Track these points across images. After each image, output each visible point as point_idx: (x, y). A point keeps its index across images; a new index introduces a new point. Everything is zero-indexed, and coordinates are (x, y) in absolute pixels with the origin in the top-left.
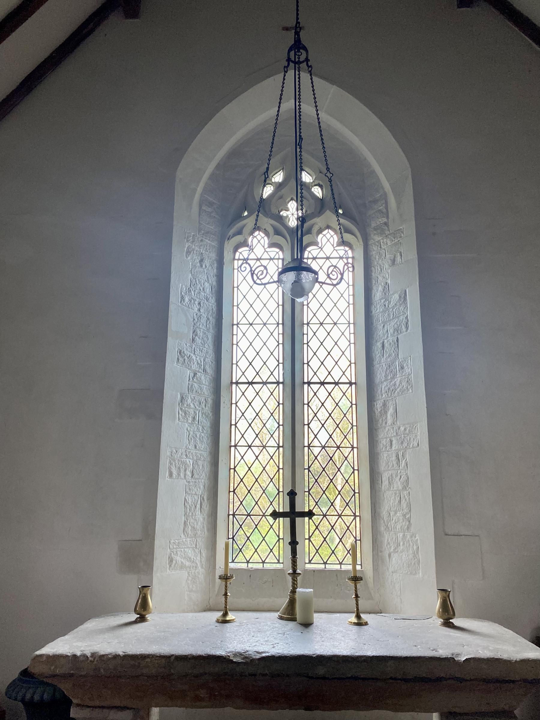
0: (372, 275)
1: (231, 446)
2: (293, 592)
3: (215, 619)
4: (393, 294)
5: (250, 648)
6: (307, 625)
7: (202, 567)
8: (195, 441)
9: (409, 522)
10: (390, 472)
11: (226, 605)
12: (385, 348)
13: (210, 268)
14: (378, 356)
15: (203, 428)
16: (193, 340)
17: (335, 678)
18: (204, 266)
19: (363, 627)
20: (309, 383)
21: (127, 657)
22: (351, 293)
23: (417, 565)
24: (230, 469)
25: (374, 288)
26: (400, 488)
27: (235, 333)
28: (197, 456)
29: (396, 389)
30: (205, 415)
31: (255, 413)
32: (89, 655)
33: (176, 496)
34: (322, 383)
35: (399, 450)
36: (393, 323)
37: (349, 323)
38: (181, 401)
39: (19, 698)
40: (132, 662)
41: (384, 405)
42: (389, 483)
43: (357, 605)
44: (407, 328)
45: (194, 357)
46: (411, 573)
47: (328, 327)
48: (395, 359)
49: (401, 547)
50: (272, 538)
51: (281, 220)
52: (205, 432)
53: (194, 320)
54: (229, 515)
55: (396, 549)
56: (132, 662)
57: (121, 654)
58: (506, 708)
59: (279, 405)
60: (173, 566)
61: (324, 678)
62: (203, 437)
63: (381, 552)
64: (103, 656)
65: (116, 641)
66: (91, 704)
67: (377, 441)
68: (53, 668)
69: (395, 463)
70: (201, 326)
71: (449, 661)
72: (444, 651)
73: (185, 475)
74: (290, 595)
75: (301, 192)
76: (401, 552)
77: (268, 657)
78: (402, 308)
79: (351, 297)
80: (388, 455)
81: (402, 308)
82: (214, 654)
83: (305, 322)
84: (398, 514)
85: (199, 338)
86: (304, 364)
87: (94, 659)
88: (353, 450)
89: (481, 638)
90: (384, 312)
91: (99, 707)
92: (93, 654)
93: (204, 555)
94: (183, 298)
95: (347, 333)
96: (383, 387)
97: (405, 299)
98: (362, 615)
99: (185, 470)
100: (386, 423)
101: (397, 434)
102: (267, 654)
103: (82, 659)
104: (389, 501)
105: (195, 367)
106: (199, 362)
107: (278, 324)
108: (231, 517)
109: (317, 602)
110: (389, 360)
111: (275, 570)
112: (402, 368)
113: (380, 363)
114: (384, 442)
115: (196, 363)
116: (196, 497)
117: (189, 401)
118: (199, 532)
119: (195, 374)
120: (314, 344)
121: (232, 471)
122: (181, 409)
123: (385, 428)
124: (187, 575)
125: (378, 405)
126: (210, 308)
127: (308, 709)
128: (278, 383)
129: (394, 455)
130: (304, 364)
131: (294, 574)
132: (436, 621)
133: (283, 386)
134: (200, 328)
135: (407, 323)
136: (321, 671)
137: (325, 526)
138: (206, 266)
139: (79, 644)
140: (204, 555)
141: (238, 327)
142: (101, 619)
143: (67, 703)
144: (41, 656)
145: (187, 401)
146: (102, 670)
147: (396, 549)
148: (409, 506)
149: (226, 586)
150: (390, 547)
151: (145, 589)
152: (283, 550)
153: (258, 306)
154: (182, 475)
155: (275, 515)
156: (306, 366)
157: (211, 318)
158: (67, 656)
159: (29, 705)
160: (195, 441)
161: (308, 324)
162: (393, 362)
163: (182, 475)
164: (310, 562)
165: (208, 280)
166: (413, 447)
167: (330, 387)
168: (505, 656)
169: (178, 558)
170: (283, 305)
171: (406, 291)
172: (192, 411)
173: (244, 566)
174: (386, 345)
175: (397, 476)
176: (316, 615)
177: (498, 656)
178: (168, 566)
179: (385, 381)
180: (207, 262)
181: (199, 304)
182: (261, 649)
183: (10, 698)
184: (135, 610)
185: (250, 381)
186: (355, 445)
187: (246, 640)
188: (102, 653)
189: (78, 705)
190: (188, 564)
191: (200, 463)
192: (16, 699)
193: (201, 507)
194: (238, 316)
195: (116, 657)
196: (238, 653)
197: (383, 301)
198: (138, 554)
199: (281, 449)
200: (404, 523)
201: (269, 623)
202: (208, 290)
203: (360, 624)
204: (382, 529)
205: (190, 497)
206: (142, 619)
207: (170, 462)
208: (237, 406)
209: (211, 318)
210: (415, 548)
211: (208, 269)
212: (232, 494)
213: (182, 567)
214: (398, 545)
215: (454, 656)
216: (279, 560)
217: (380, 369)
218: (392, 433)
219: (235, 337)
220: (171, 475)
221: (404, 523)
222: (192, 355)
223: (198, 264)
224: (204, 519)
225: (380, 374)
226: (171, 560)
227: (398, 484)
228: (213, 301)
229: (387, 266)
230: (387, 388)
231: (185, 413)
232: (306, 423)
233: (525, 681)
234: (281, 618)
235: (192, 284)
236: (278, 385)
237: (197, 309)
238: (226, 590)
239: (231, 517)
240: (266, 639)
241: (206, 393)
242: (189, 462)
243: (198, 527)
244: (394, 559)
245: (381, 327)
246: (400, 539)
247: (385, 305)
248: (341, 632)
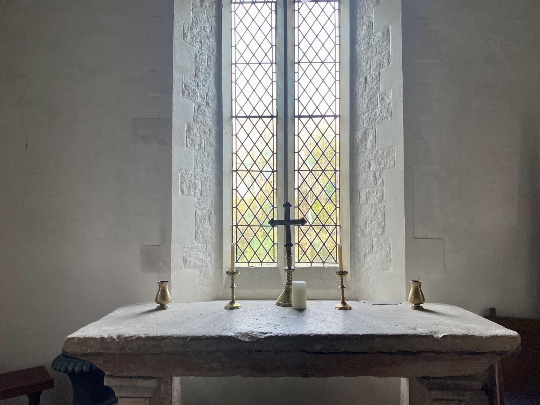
0: (357, 16)
1: (233, 171)
2: (289, 283)
3: (224, 306)
4: (377, 32)
5: (256, 330)
6: (301, 310)
7: (212, 267)
8: (202, 165)
9: (383, 229)
10: (368, 190)
11: (233, 295)
12: (368, 82)
13: (210, 9)
14: (360, 90)
15: (208, 154)
16: (196, 75)
17: (330, 353)
18: (204, 7)
19: (348, 311)
20: (299, 117)
21: (148, 339)
22: (337, 34)
23: (388, 262)
24: (233, 189)
25: (359, 28)
26: (376, 201)
27: (233, 71)
28: (205, 178)
29: (376, 119)
30: (210, 143)
31: (252, 143)
32: (115, 337)
33: (187, 211)
34: (311, 117)
35: (376, 170)
36: (375, 59)
37: (335, 62)
38: (188, 130)
39: (62, 369)
40: (153, 343)
41: (365, 133)
42: (367, 198)
43: (343, 293)
44: (389, 62)
45: (198, 91)
46: (383, 269)
47: (317, 66)
48: (376, 92)
49: (376, 249)
52: (210, 158)
53: (197, 56)
54: (233, 226)
55: (370, 250)
56: (153, 343)
57: (143, 336)
58: (472, 373)
59: (273, 136)
60: (187, 265)
61: (320, 353)
62: (208, 162)
63: (358, 253)
64: (128, 338)
65: (140, 325)
66: (120, 375)
67: (357, 165)
68: (84, 348)
69: (372, 181)
70: (203, 63)
71: (429, 338)
72: (423, 330)
73: (195, 193)
74: (286, 287)
76: (375, 253)
77: (272, 336)
78: (384, 44)
79: (337, 38)
80: (367, 176)
81: (384, 44)
82: (224, 335)
83: (296, 61)
84: (373, 223)
85: (202, 74)
86: (295, 99)
87: (120, 340)
88: (335, 173)
89: (450, 318)
90: (368, 49)
91: (128, 377)
92: (119, 337)
93: (213, 257)
94: (185, 35)
95: (333, 71)
96: (365, 118)
97: (388, 35)
98: (346, 302)
99: (195, 189)
100: (366, 149)
101: (375, 157)
102: (271, 335)
103: (109, 340)
104: (366, 212)
105: (199, 100)
106: (203, 96)
107: (272, 63)
108: (234, 227)
109: (309, 293)
110: (371, 93)
111: (271, 268)
112: (383, 99)
113: (362, 97)
114: (363, 165)
115: (200, 97)
116: (205, 211)
117: (195, 130)
118: (208, 239)
119: (199, 107)
120: (304, 81)
121: (234, 191)
122: (189, 137)
123: (365, 153)
124: (199, 272)
125: (360, 134)
126: (211, 47)
127: (305, 376)
128: (272, 117)
129: (372, 175)
130: (295, 99)
131: (290, 270)
132: (407, 306)
133: (277, 119)
134: (202, 65)
135: (389, 58)
136: (318, 347)
138: (206, 7)
139: (107, 328)
140: (213, 257)
141: (236, 66)
142: (127, 308)
143: (100, 375)
144: (73, 339)
145: (193, 130)
146: (127, 349)
147: (370, 250)
148: (384, 216)
149: (233, 280)
150: (366, 249)
151: (164, 284)
152: (279, 253)
153: (254, 46)
154: (192, 193)
155: (273, 223)
156: (296, 101)
157: (212, 56)
158: (96, 338)
159: (72, 375)
160: (202, 165)
161: (299, 63)
162: (374, 95)
163: (192, 193)
164: (299, 262)
165: (208, 19)
166: (389, 167)
167: (317, 120)
168: (477, 333)
169: (192, 260)
170: (276, 46)
171: (389, 28)
172: (198, 140)
173: (246, 265)
174: (369, 79)
175: (373, 192)
176: (308, 302)
177: (470, 333)
178: (183, 266)
179: (366, 112)
181: (201, 42)
182: (265, 330)
183: (55, 370)
184: (156, 301)
185: (248, 115)
186: (338, 169)
187: (251, 323)
188: (127, 336)
189: (110, 376)
190: (200, 264)
191: (207, 183)
192: (60, 371)
193: (209, 219)
194: (235, 56)
195: (139, 338)
196: (246, 333)
197: (366, 39)
198: (157, 257)
199: (275, 173)
200: (378, 230)
201: (269, 309)
202: (208, 29)
203: (345, 308)
204: (359, 235)
205: (200, 211)
206: (162, 307)
207: (181, 182)
208: (237, 137)
209: (212, 56)
210: (387, 249)
211: (208, 10)
212: (234, 209)
214: (373, 247)
215: (432, 334)
216: (274, 261)
217: (363, 102)
218: (371, 156)
219: (233, 75)
220: (182, 192)
221: (378, 230)
222: (196, 89)
223: (199, 4)
224: (212, 229)
225: (362, 106)
226: (186, 261)
227: (374, 199)
228: (213, 40)
229: (371, 6)
230: (368, 118)
231: (192, 141)
232: (296, 151)
233: (494, 353)
234: (279, 305)
235: (194, 23)
236: (272, 118)
237: (198, 47)
238: (233, 283)
239: (234, 227)
240: (268, 322)
241: (210, 124)
242: (198, 182)
243: (208, 235)
244: (368, 259)
245: (365, 64)
246: (374, 243)
247: (369, 43)
248: (331, 315)
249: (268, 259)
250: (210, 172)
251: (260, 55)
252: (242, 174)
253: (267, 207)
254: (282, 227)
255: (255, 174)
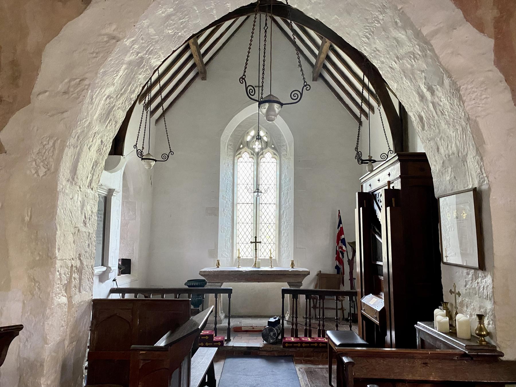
31: (244, 213)
50: (249, 250)
51: (253, 149)
75: (259, 138)
125: (282, 212)
137: (265, 246)
180: (230, 165)
213: (225, 257)
225: (283, 202)
227: (286, 235)
249: (249, 255)
250: (230, 223)
251: (247, 220)
252: (241, 224)
253: (250, 237)
254: (254, 244)
255: (245, 242)
